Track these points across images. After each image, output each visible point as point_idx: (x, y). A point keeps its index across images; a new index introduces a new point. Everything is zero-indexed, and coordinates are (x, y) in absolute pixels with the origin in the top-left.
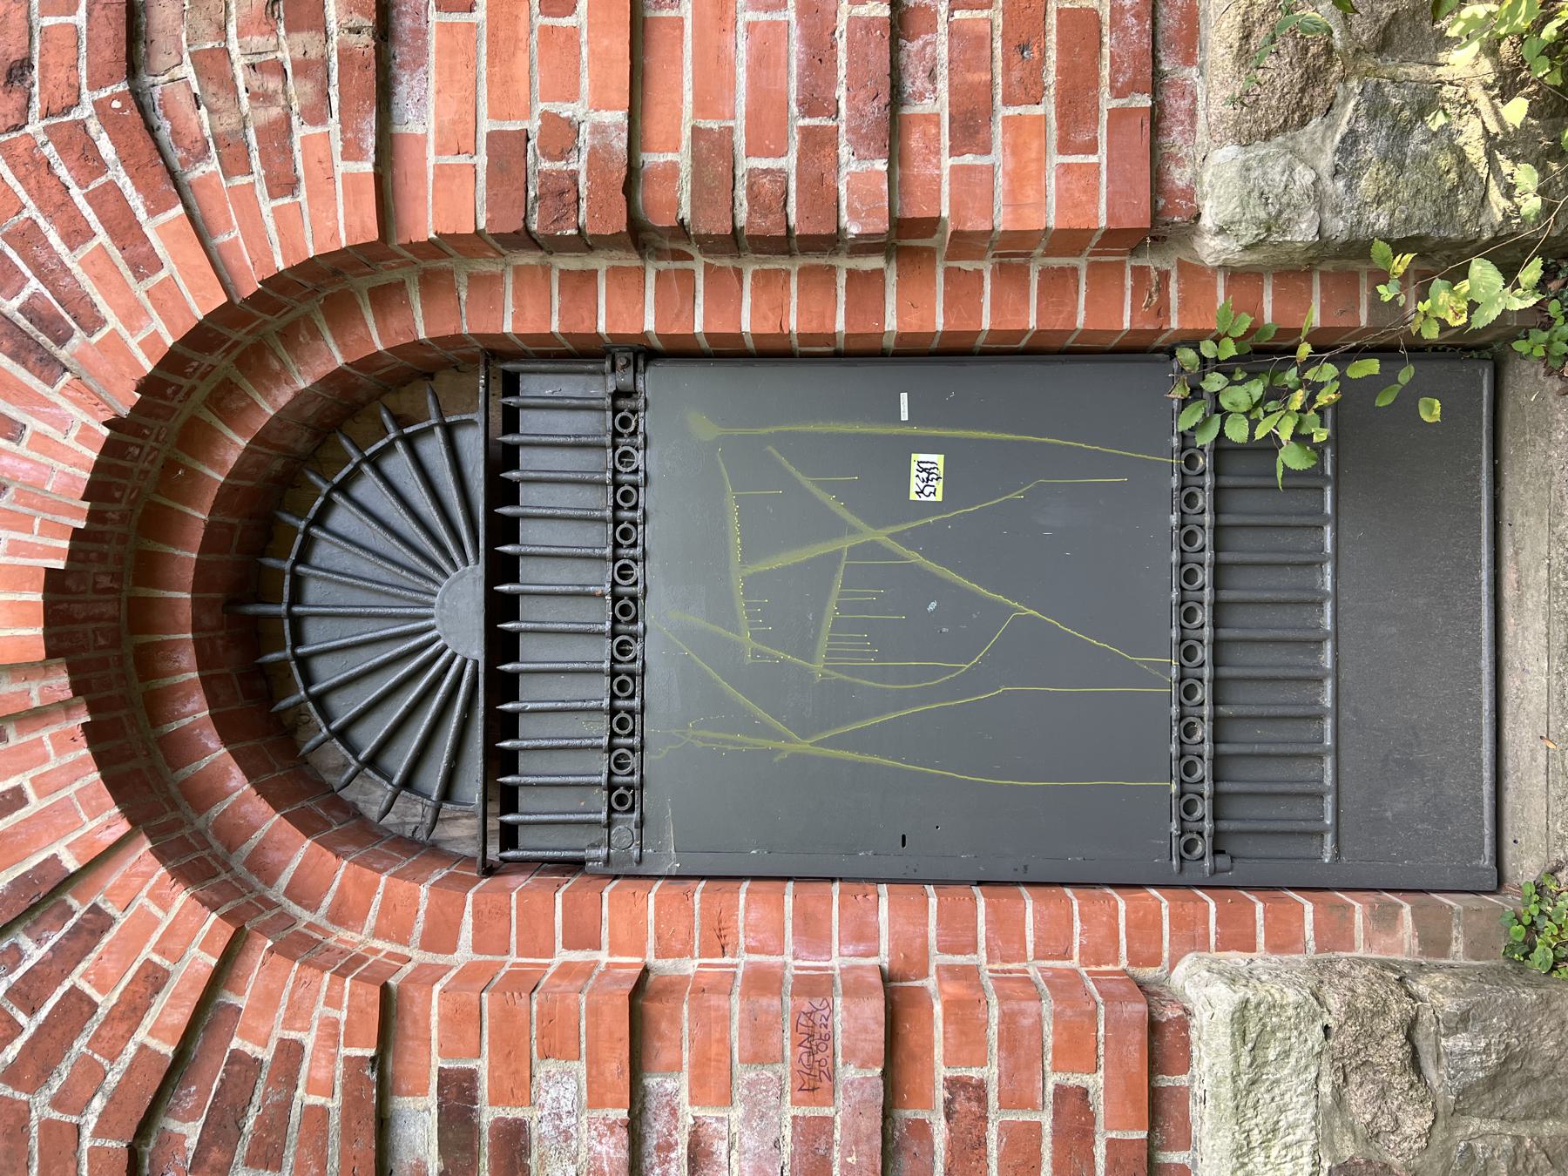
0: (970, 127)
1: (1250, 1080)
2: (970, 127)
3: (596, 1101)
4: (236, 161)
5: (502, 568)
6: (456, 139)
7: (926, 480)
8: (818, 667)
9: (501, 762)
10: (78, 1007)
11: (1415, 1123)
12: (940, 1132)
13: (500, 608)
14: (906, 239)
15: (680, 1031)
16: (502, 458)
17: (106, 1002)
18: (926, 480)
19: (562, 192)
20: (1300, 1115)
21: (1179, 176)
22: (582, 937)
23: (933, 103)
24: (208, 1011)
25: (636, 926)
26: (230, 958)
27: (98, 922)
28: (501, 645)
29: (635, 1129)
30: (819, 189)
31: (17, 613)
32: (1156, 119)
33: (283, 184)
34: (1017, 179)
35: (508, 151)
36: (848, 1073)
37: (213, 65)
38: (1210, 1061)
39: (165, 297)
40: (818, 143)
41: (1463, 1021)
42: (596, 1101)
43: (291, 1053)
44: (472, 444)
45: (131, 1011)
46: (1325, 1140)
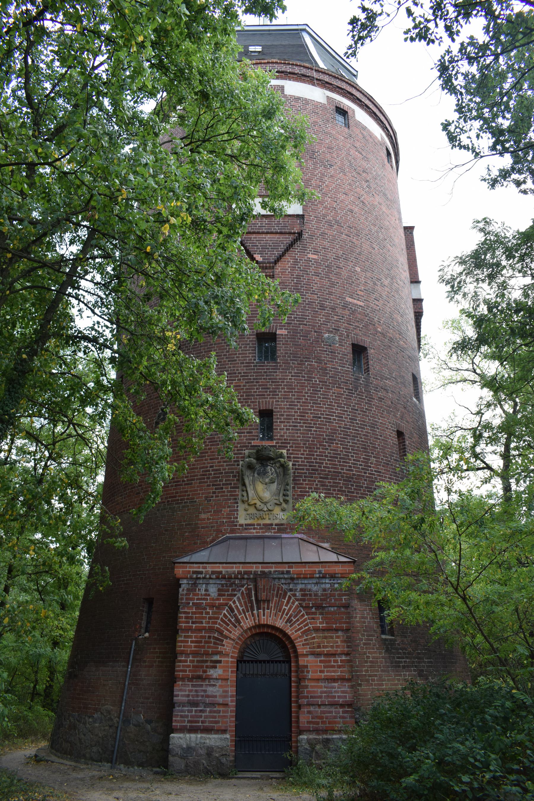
0: (309, 712)
1: (221, 739)
2: (309, 712)
5: (268, 662)
6: (308, 661)
13: (264, 661)
14: (299, 707)
15: (224, 683)
16: (280, 662)
19: (303, 672)
23: (312, 709)
27: (236, 627)
28: (260, 662)
32: (310, 731)
33: (303, 645)
35: (306, 667)
40: (307, 697)
44: (281, 659)
45: (228, 630)
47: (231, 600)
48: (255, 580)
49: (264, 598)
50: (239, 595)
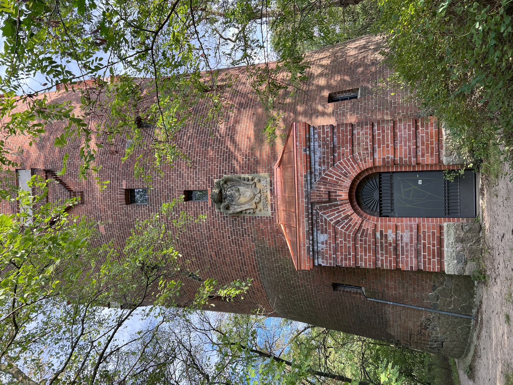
0: (423, 156)
1: (448, 231)
2: (423, 156)
3: (393, 232)
4: (361, 160)
5: (380, 191)
7: (420, 182)
8: (410, 199)
9: (381, 207)
10: (350, 225)
11: (463, 234)
12: (422, 235)
17: (353, 225)
18: (420, 182)
20: (453, 233)
21: (441, 159)
22: (390, 221)
23: (420, 154)
24: (361, 226)
25: (393, 222)
26: (363, 221)
27: (352, 219)
28: (380, 197)
29: (396, 234)
30: (410, 161)
31: (346, 196)
32: (439, 155)
33: (365, 162)
34: (427, 160)
36: (414, 230)
37: (359, 154)
38: (445, 229)
39: (356, 171)
40: (410, 158)
41: (466, 226)
42: (393, 232)
43: (368, 229)
44: (378, 180)
45: (354, 226)
46: (455, 235)
47: (330, 223)
48: (312, 204)
49: (327, 196)
50: (325, 216)
